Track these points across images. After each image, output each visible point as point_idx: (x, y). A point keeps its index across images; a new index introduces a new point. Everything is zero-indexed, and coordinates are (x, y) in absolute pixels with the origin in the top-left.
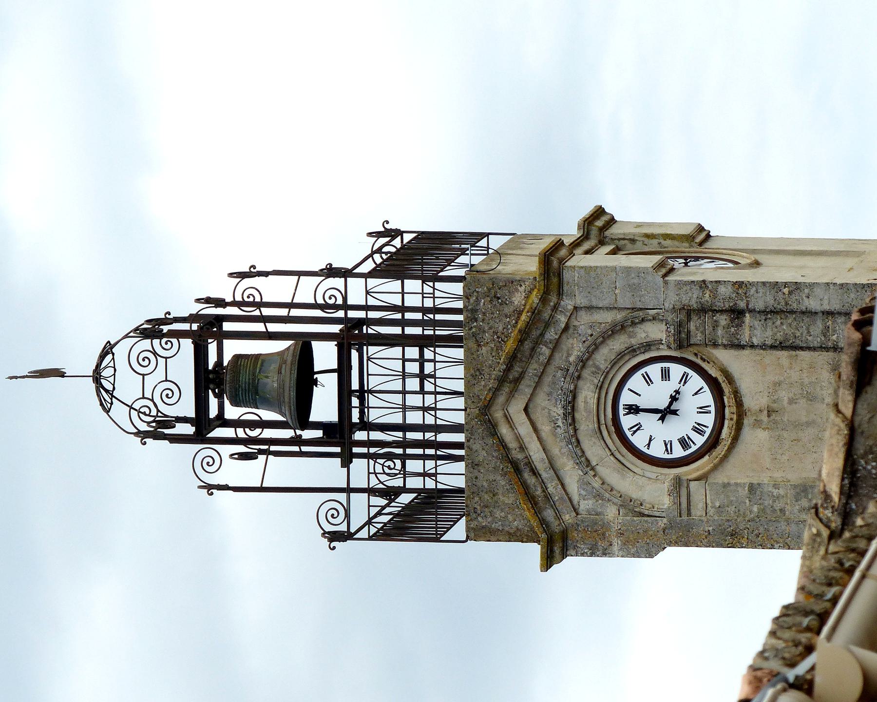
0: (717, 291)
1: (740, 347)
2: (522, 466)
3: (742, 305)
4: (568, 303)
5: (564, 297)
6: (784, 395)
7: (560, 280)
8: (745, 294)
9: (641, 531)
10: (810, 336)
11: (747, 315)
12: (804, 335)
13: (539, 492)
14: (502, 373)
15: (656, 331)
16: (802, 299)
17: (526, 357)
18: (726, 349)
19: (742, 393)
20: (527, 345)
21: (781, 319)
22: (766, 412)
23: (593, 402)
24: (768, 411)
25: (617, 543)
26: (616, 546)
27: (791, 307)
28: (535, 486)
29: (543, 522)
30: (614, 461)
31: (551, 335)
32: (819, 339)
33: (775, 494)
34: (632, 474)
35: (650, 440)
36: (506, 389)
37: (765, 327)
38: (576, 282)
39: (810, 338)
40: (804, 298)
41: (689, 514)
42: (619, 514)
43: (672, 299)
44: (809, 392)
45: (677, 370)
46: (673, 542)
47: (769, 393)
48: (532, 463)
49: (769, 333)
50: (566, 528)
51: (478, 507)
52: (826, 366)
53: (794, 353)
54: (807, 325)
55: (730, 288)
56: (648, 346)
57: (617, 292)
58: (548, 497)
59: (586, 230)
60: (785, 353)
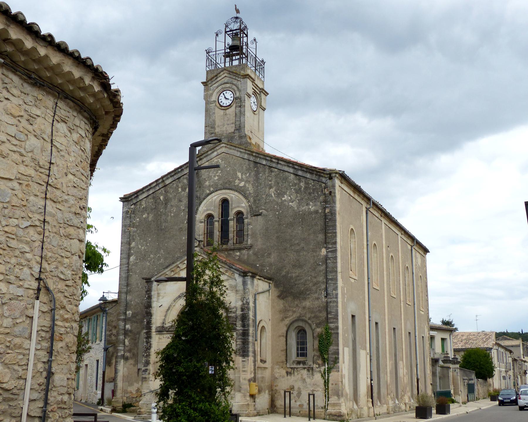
3: (241, 107)
4: (242, 80)
6: (228, 116)
13: (213, 80)
15: (238, 95)
20: (235, 74)
25: (206, 93)
31: (237, 78)
56: (236, 94)
58: (212, 82)
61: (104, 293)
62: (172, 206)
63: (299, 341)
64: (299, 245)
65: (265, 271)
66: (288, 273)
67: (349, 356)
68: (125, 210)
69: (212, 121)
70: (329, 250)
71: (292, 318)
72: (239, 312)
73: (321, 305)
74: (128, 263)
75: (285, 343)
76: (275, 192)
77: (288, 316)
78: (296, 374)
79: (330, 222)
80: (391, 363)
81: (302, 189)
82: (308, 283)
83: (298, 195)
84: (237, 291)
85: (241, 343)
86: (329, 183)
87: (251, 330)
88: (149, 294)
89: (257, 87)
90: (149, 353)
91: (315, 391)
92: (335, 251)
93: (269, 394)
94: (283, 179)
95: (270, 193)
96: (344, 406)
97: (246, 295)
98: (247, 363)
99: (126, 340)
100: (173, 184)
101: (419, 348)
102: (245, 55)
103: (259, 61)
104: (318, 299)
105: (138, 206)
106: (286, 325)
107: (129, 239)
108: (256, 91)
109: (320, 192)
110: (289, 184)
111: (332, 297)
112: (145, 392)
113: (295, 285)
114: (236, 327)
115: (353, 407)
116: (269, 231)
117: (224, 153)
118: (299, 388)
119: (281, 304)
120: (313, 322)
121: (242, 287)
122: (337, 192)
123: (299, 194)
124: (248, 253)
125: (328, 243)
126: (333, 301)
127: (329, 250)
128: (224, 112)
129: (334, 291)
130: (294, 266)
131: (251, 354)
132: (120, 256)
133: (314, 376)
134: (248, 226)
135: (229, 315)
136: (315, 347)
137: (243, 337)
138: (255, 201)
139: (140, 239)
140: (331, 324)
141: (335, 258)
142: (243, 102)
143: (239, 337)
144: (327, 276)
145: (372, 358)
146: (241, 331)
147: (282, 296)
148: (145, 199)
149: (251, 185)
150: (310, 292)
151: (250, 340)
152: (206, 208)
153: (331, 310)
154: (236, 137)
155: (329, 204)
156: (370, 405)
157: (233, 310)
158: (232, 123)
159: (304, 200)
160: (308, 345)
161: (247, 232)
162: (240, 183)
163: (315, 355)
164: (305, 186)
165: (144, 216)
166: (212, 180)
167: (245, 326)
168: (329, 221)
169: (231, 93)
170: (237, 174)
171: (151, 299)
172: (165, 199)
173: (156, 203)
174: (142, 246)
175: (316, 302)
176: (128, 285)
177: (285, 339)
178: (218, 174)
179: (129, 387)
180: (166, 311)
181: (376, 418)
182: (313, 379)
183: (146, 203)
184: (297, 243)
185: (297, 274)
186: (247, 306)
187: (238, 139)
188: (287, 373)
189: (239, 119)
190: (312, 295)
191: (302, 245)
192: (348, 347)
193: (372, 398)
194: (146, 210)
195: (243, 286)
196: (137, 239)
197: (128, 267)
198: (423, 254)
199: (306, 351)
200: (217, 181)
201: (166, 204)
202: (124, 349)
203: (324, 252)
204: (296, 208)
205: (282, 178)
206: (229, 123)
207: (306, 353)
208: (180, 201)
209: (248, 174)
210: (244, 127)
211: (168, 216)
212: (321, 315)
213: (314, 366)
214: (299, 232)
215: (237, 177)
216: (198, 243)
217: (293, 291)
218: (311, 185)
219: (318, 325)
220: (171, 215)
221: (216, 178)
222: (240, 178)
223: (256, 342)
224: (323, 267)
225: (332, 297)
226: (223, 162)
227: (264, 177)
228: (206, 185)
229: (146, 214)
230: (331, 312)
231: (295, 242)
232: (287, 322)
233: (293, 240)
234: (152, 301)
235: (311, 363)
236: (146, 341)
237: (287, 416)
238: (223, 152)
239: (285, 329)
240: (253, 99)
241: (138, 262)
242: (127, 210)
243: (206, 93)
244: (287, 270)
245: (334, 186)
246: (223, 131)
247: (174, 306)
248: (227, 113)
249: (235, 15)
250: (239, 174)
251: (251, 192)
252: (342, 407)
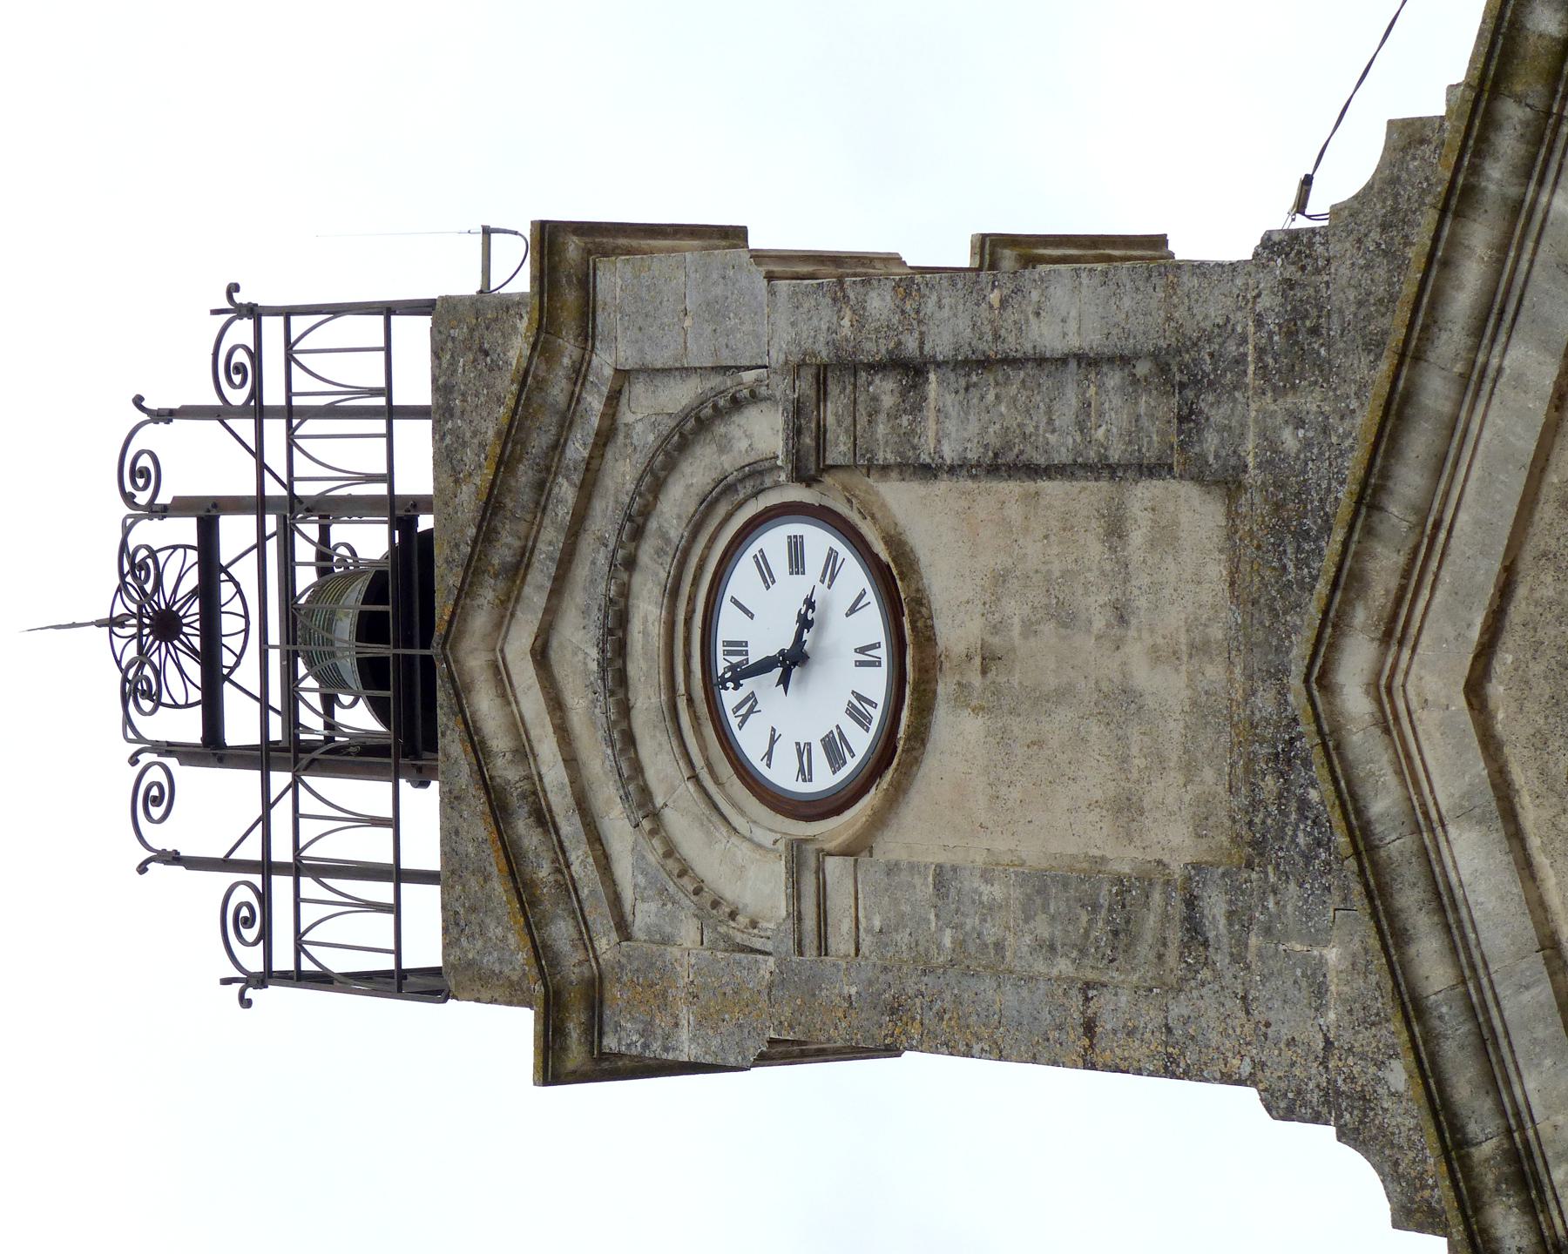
0: (864, 309)
1: (928, 471)
2: (514, 800)
4: (604, 363)
5: (598, 344)
7: (588, 293)
8: (918, 312)
9: (728, 990)
10: (1053, 431)
11: (932, 377)
12: (1041, 432)
13: (544, 872)
14: (469, 549)
16: (1027, 320)
17: (523, 507)
18: (904, 480)
19: (933, 607)
20: (524, 475)
21: (997, 384)
22: (977, 661)
23: (657, 630)
24: (984, 659)
26: (685, 1030)
27: (1006, 346)
28: (537, 856)
29: (541, 952)
30: (695, 795)
31: (577, 449)
32: (1071, 441)
33: (985, 898)
34: (724, 830)
35: (773, 741)
36: (488, 594)
37: (965, 408)
38: (618, 301)
39: (1052, 438)
40: (1031, 316)
41: (823, 948)
42: (702, 943)
44: (1061, 600)
45: (819, 541)
46: (786, 1024)
47: (984, 604)
48: (541, 794)
49: (973, 427)
50: (600, 975)
51: (462, 911)
52: (1094, 523)
53: (1030, 486)
54: (1047, 400)
55: (888, 298)
56: (756, 474)
57: (688, 323)
58: (568, 887)
59: (987, 257)
60: (1011, 488)
117: (1497, 690)
142: (860, 323)
154: (1290, 440)
206: (1094, 605)
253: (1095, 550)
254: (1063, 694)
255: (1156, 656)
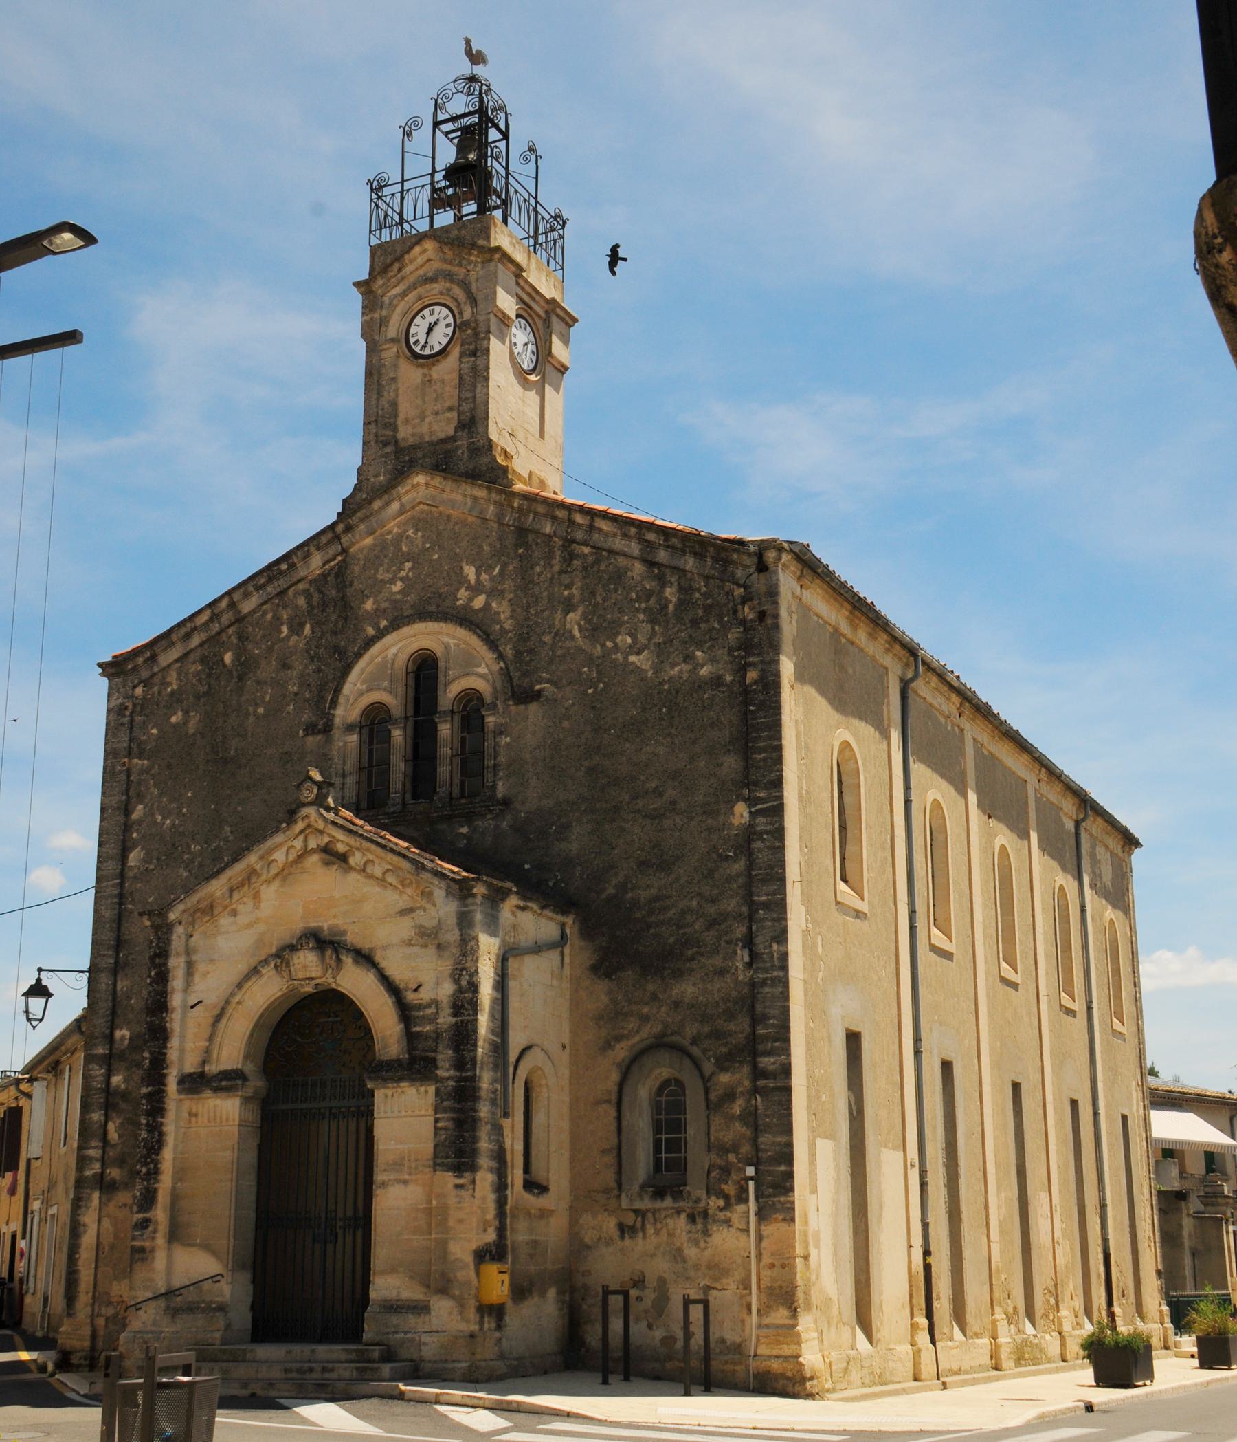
3: (478, 354)
6: (438, 387)
15: (467, 314)
25: (367, 318)
43: (481, 318)
56: (461, 313)
61: (40, 970)
62: (258, 682)
63: (663, 1117)
64: (661, 795)
65: (551, 884)
66: (623, 887)
67: (837, 1167)
68: (113, 703)
69: (386, 406)
70: (759, 807)
71: (637, 1039)
72: (446, 1019)
73: (735, 994)
74: (122, 875)
75: (613, 1127)
76: (582, 623)
77: (625, 1032)
78: (650, 1230)
79: (762, 713)
80: (1003, 1195)
81: (671, 607)
82: (689, 918)
83: (657, 628)
84: (439, 946)
85: (450, 1124)
86: (759, 583)
87: (486, 1080)
88: (160, 965)
89: (534, 294)
90: (156, 1163)
91: (713, 1288)
92: (778, 810)
93: (563, 1302)
94: (609, 579)
95: (568, 626)
96: (816, 1342)
97: (469, 959)
98: (471, 1191)
99: (111, 1127)
100: (265, 613)
101: (1109, 1151)
102: (499, 197)
103: (547, 217)
104: (722, 972)
105: (156, 689)
106: (619, 1065)
107: (127, 794)
108: (531, 308)
109: (728, 615)
110: (628, 593)
111: (769, 965)
112: (140, 1300)
113: (649, 926)
114: (437, 1068)
115: (853, 1347)
116: (564, 753)
118: (662, 1281)
119: (600, 994)
120: (704, 1051)
121: (457, 932)
122: (783, 613)
123: (660, 625)
124: (497, 827)
125: (756, 784)
126: (773, 979)
127: (759, 807)
128: (425, 376)
129: (775, 946)
130: (643, 865)
131: (484, 1161)
132: (99, 852)
133: (710, 1236)
134: (498, 740)
135: (414, 1029)
136: (712, 1139)
137: (459, 1103)
138: (518, 654)
139: (160, 795)
140: (766, 1059)
141: (779, 833)
142: (483, 339)
143: (446, 1104)
144: (750, 894)
145: (929, 1178)
146: (451, 1083)
147: (604, 967)
148: (178, 665)
149: (505, 603)
150: (695, 950)
151: (482, 1115)
152: (364, 686)
153: (767, 1010)
154: (460, 451)
155: (759, 655)
156: (923, 1338)
157: (429, 1011)
158: (450, 409)
159: (676, 643)
160: (691, 1131)
161: (495, 759)
162: (471, 599)
163: (714, 1166)
164: (679, 599)
165: (174, 719)
166: (385, 594)
167: (466, 1064)
168: (758, 710)
169: (447, 312)
170: (461, 568)
171: (167, 981)
172: (239, 660)
173: (209, 675)
174: (164, 818)
175: (717, 984)
176: (119, 944)
177: (613, 1113)
178: (403, 574)
179: (115, 1283)
180: (211, 1020)
181: (944, 1384)
182: (706, 1248)
183: (179, 678)
184: (656, 788)
185: (654, 891)
186: (471, 995)
187: (465, 456)
188: (622, 1228)
189: (469, 395)
190: (703, 960)
191: (670, 793)
192: (831, 1136)
193: (929, 1315)
194: (179, 701)
195: (460, 930)
196: (152, 794)
197: (121, 885)
198: (1119, 851)
199: (685, 1152)
200: (399, 597)
201: (240, 678)
202: (103, 1157)
203: (741, 813)
204: (650, 673)
205: (606, 576)
206: (438, 407)
207: (685, 1158)
208: (285, 666)
209: (497, 570)
210: (487, 417)
211: (248, 714)
212: (732, 1026)
213: (712, 1204)
214: (661, 750)
215: (463, 580)
216: (315, 791)
217: (641, 948)
218: (697, 595)
219: (724, 1063)
220: (255, 711)
221: (398, 586)
222: (473, 582)
223: (506, 1123)
224: (740, 866)
225: (769, 965)
226: (420, 534)
227: (549, 575)
228: (366, 611)
229: (180, 713)
230: (765, 1017)
231: (648, 785)
232: (622, 1051)
233: (642, 778)
234: (169, 988)
235: (702, 1193)
236: (147, 1125)
237: (611, 1378)
238: (420, 503)
239: (615, 1076)
240: (520, 336)
241: (151, 867)
242: (120, 701)
243: (367, 318)
244: (621, 878)
245: (773, 593)
246: (421, 436)
247: (238, 1003)
248: (435, 376)
249: (466, 68)
250: (470, 572)
251: (507, 628)
252: (803, 1345)
253: (447, 404)
254: (424, 402)
255: (430, 423)
